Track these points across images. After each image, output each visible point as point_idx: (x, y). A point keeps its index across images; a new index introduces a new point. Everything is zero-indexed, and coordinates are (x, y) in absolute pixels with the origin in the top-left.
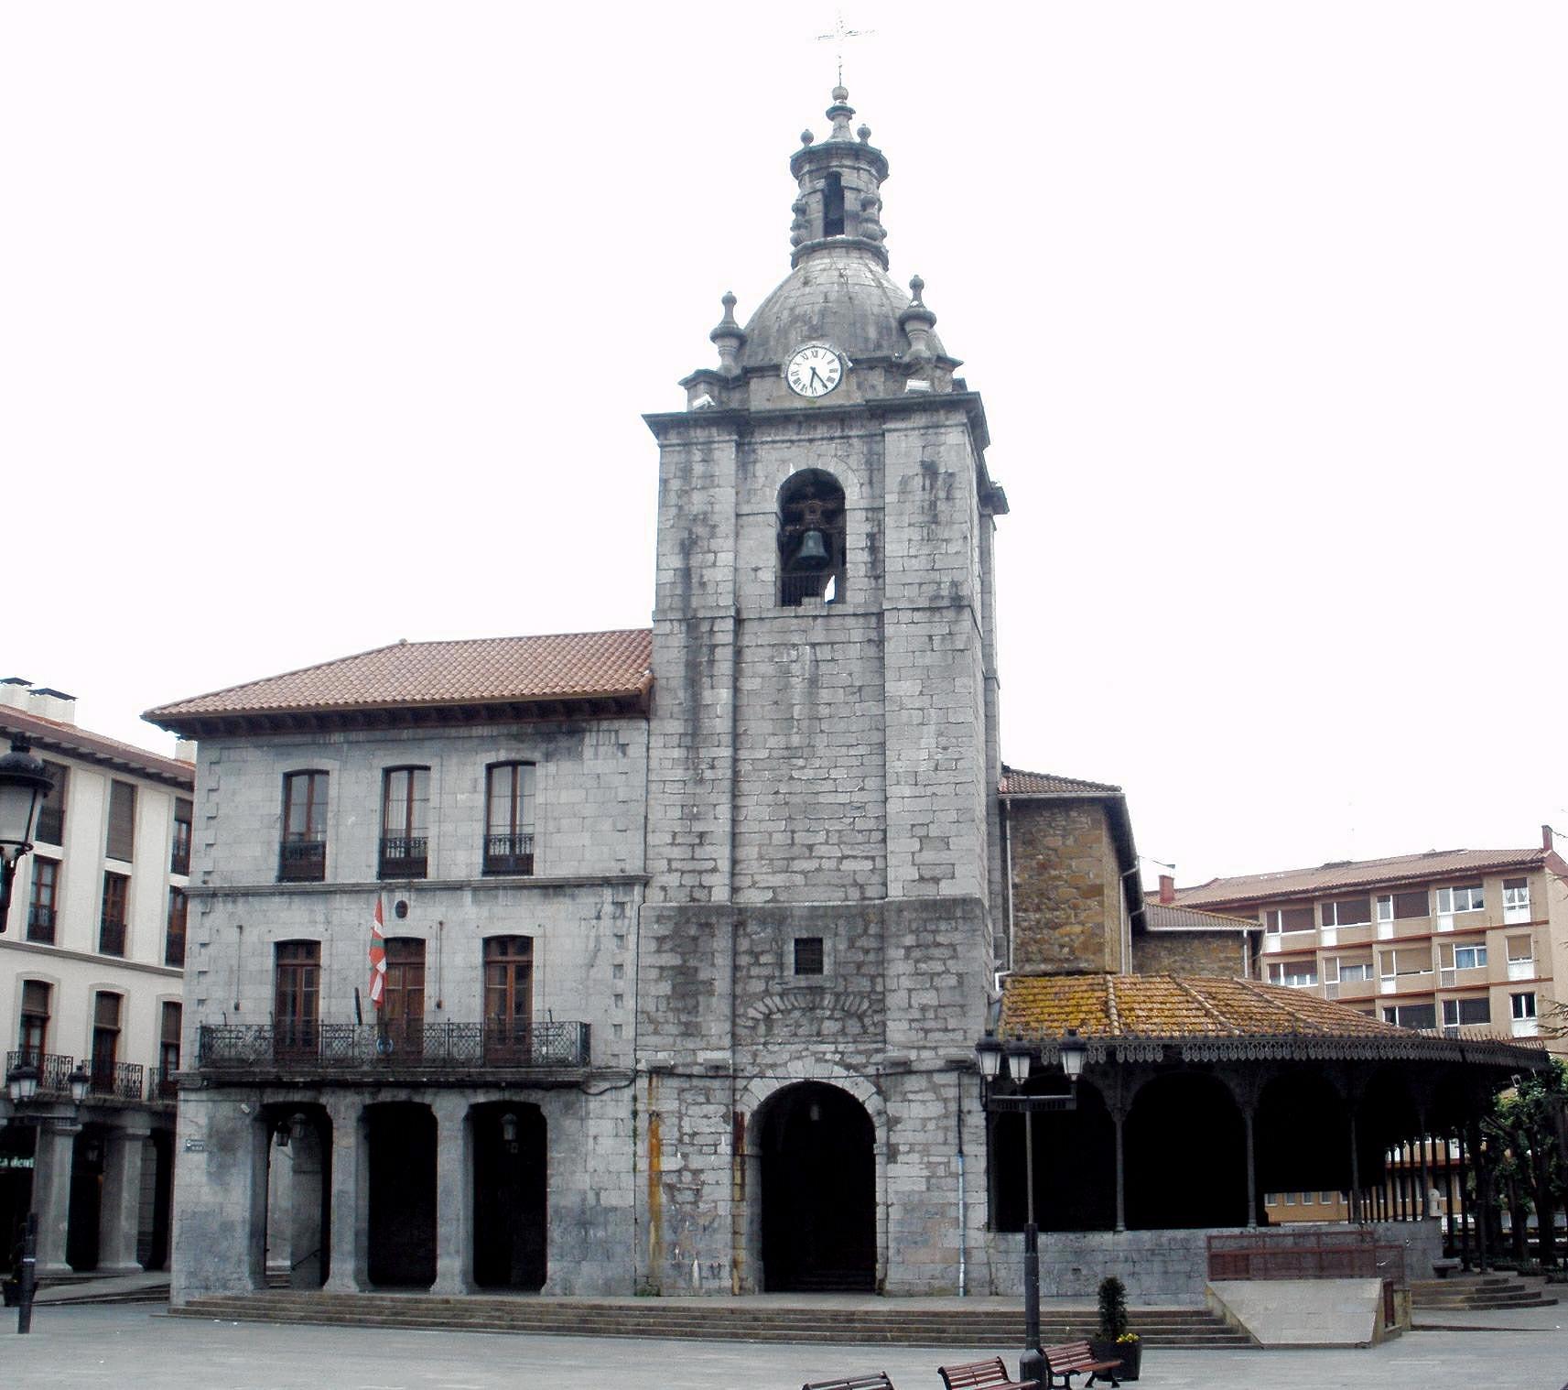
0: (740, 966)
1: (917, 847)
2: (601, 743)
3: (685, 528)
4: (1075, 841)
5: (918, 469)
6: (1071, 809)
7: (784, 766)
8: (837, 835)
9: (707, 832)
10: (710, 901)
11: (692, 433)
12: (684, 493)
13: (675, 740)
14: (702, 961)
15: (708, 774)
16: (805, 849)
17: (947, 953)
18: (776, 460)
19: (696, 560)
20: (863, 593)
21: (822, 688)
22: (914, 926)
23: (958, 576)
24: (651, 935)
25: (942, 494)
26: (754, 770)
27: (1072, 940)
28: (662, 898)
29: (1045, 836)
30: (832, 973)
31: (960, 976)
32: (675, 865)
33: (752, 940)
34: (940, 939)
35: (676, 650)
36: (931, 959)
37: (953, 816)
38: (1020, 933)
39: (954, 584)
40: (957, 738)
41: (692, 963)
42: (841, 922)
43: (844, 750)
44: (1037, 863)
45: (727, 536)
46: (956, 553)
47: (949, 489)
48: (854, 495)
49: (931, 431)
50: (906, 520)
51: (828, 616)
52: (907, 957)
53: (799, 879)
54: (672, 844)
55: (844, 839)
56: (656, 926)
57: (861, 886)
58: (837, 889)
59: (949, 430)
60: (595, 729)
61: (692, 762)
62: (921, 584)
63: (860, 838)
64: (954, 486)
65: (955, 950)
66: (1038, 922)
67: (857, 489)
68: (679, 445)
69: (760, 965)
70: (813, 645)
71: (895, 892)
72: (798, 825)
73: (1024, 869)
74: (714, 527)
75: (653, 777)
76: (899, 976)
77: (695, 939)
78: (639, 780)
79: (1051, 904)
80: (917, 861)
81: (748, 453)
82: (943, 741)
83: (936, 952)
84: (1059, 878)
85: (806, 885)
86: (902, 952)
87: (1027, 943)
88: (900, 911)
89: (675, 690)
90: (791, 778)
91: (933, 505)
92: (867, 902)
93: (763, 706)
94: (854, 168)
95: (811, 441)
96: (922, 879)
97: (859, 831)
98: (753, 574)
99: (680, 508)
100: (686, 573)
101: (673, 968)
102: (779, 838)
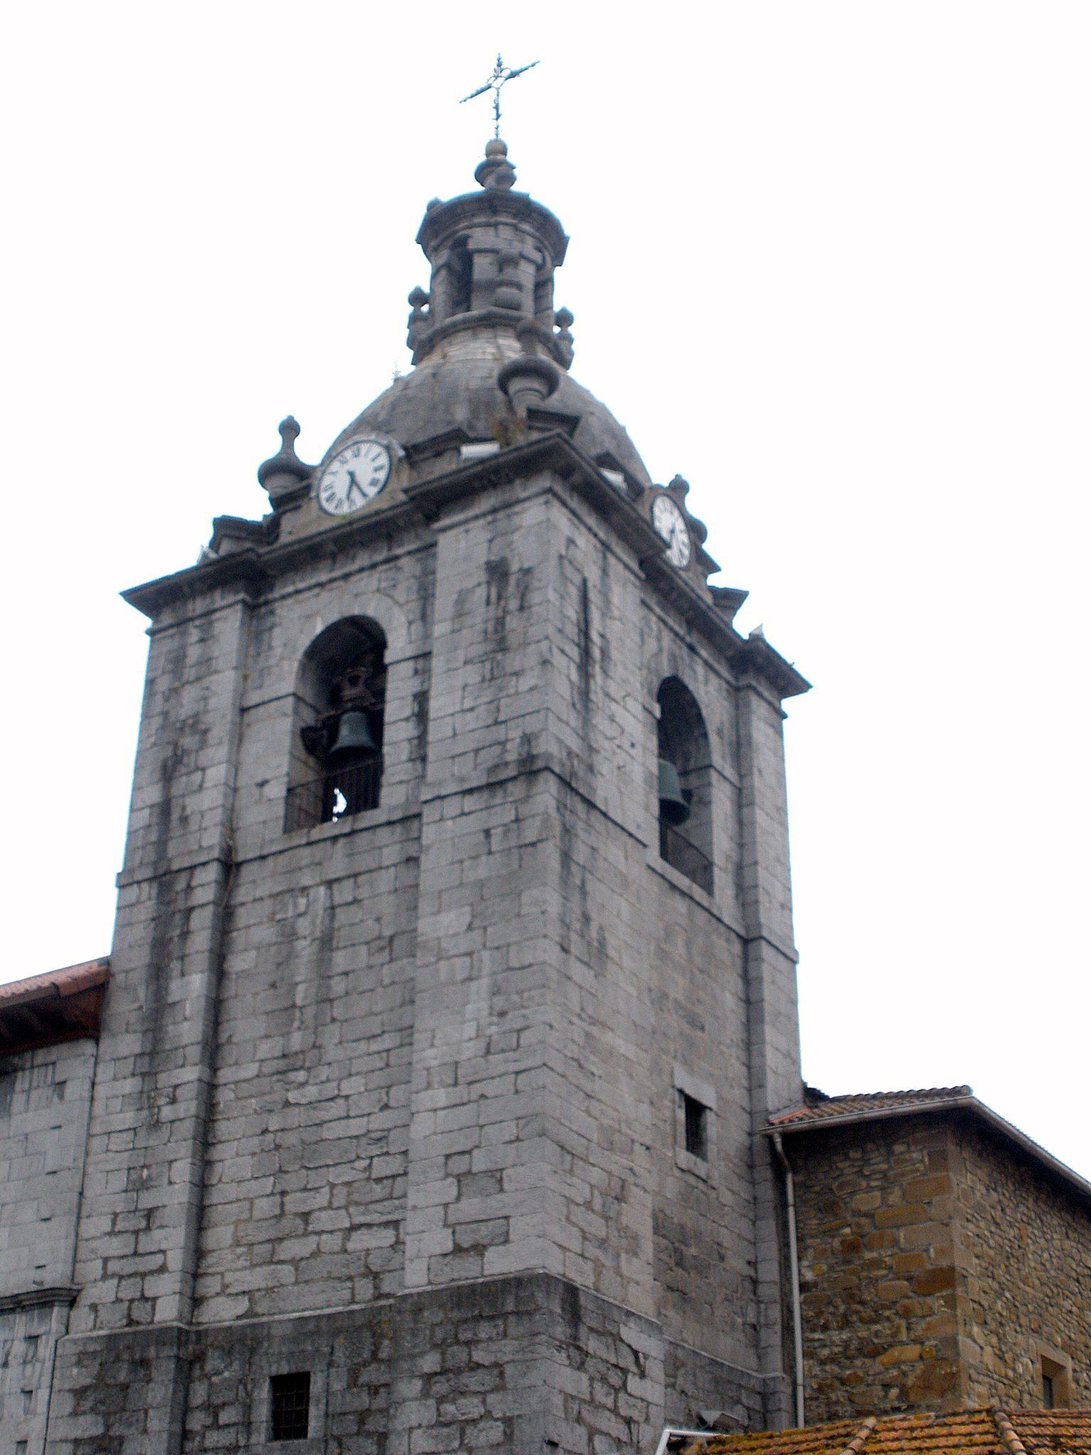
0: (191, 1431)
1: (454, 1192)
2: (35, 1084)
3: (168, 743)
4: (903, 1197)
5: (482, 576)
6: (895, 1141)
7: (278, 1086)
8: (345, 1190)
9: (157, 1208)
10: (152, 1322)
11: (190, 606)
12: (174, 692)
13: (128, 1066)
14: (130, 1425)
15: (167, 1113)
16: (298, 1221)
17: (489, 1379)
18: (300, 617)
19: (178, 787)
20: (404, 786)
21: (338, 948)
22: (439, 1334)
23: (532, 724)
24: (67, 1386)
25: (513, 604)
26: (238, 1099)
27: (905, 1374)
28: (91, 1324)
29: (852, 1193)
30: (320, 1434)
31: (508, 1421)
32: (113, 1267)
33: (211, 1385)
34: (479, 1356)
35: (141, 926)
36: (463, 1394)
37: (510, 1130)
38: (817, 1370)
39: (527, 739)
40: (520, 993)
41: (116, 1431)
42: (340, 1342)
43: (363, 1046)
44: (842, 1242)
45: (220, 743)
46: (532, 689)
47: (524, 592)
48: (398, 645)
49: (501, 515)
50: (461, 655)
51: (352, 833)
52: (425, 1394)
53: (287, 1273)
54: (112, 1233)
55: (356, 1197)
56: (75, 1371)
57: (376, 1276)
58: (338, 1285)
59: (527, 505)
60: (28, 1065)
61: (147, 1099)
62: (477, 751)
63: (378, 1191)
64: (531, 587)
65: (502, 1374)
66: (846, 1344)
67: (404, 631)
68: (171, 626)
69: (219, 1427)
70: (329, 884)
71: (415, 1278)
72: (293, 1181)
73: (821, 1254)
74: (206, 732)
75: (97, 1129)
76: (411, 1429)
77: (125, 1387)
78: (73, 1133)
79: (868, 1313)
80: (452, 1219)
81: (260, 618)
82: (499, 1002)
83: (473, 1381)
84: (876, 1264)
85: (296, 1283)
86: (418, 1384)
87: (831, 1387)
88: (418, 1310)
89: (135, 989)
90: (287, 1104)
91: (500, 622)
92: (383, 1302)
93: (255, 994)
94: (488, 225)
95: (346, 577)
96: (458, 1250)
97: (379, 1180)
98: (256, 791)
99: (165, 714)
100: (164, 809)
101: (92, 1440)
102: (265, 1207)
